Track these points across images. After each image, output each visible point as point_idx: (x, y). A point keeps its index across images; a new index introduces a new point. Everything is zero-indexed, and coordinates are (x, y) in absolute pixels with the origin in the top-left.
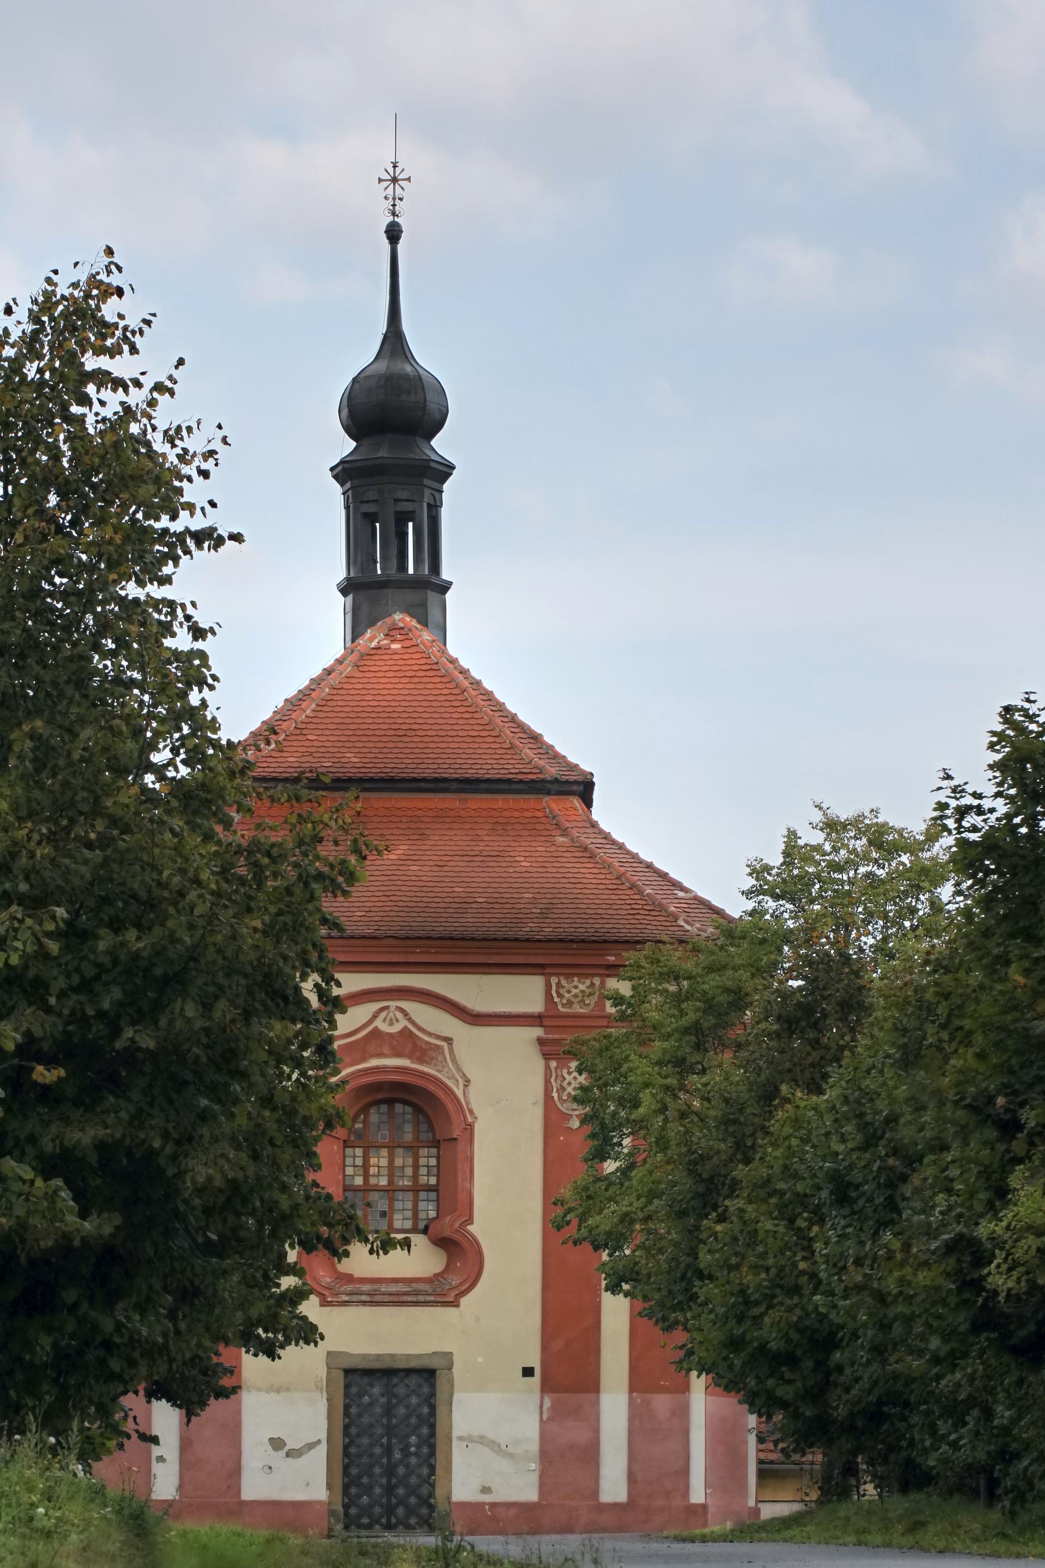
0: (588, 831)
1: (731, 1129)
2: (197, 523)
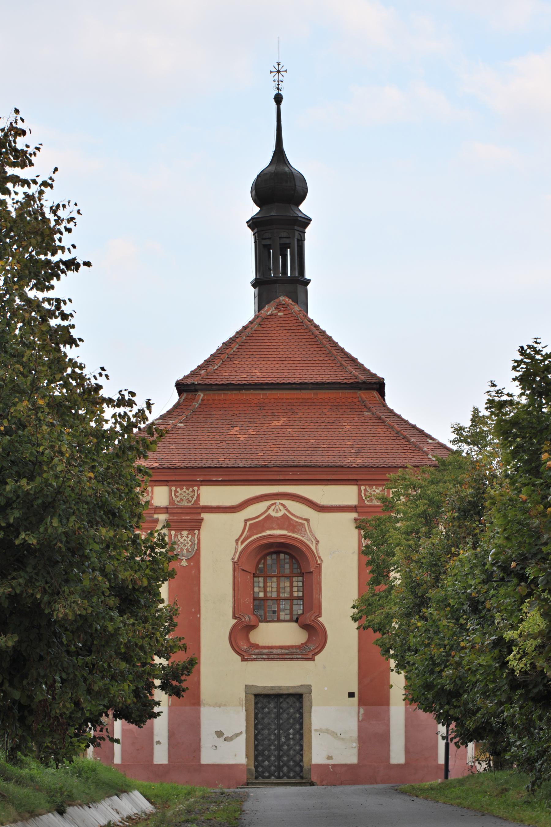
0: (381, 408)
1: (433, 569)
2: (66, 257)
